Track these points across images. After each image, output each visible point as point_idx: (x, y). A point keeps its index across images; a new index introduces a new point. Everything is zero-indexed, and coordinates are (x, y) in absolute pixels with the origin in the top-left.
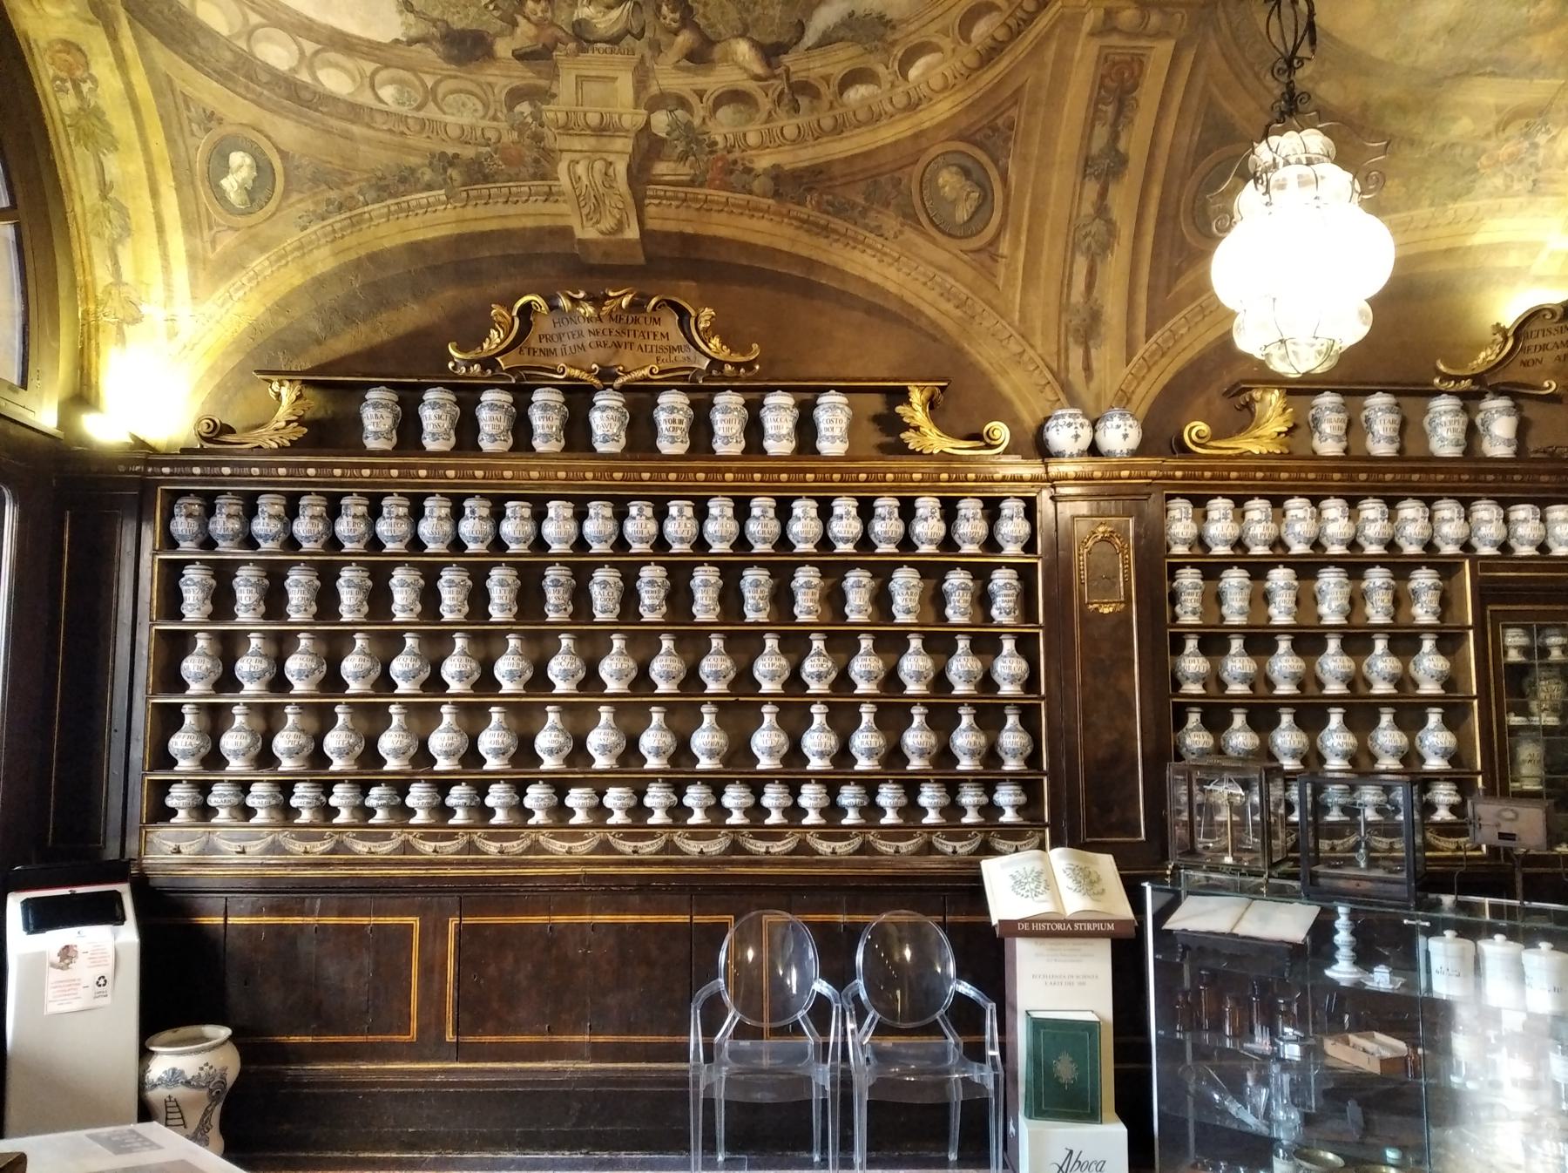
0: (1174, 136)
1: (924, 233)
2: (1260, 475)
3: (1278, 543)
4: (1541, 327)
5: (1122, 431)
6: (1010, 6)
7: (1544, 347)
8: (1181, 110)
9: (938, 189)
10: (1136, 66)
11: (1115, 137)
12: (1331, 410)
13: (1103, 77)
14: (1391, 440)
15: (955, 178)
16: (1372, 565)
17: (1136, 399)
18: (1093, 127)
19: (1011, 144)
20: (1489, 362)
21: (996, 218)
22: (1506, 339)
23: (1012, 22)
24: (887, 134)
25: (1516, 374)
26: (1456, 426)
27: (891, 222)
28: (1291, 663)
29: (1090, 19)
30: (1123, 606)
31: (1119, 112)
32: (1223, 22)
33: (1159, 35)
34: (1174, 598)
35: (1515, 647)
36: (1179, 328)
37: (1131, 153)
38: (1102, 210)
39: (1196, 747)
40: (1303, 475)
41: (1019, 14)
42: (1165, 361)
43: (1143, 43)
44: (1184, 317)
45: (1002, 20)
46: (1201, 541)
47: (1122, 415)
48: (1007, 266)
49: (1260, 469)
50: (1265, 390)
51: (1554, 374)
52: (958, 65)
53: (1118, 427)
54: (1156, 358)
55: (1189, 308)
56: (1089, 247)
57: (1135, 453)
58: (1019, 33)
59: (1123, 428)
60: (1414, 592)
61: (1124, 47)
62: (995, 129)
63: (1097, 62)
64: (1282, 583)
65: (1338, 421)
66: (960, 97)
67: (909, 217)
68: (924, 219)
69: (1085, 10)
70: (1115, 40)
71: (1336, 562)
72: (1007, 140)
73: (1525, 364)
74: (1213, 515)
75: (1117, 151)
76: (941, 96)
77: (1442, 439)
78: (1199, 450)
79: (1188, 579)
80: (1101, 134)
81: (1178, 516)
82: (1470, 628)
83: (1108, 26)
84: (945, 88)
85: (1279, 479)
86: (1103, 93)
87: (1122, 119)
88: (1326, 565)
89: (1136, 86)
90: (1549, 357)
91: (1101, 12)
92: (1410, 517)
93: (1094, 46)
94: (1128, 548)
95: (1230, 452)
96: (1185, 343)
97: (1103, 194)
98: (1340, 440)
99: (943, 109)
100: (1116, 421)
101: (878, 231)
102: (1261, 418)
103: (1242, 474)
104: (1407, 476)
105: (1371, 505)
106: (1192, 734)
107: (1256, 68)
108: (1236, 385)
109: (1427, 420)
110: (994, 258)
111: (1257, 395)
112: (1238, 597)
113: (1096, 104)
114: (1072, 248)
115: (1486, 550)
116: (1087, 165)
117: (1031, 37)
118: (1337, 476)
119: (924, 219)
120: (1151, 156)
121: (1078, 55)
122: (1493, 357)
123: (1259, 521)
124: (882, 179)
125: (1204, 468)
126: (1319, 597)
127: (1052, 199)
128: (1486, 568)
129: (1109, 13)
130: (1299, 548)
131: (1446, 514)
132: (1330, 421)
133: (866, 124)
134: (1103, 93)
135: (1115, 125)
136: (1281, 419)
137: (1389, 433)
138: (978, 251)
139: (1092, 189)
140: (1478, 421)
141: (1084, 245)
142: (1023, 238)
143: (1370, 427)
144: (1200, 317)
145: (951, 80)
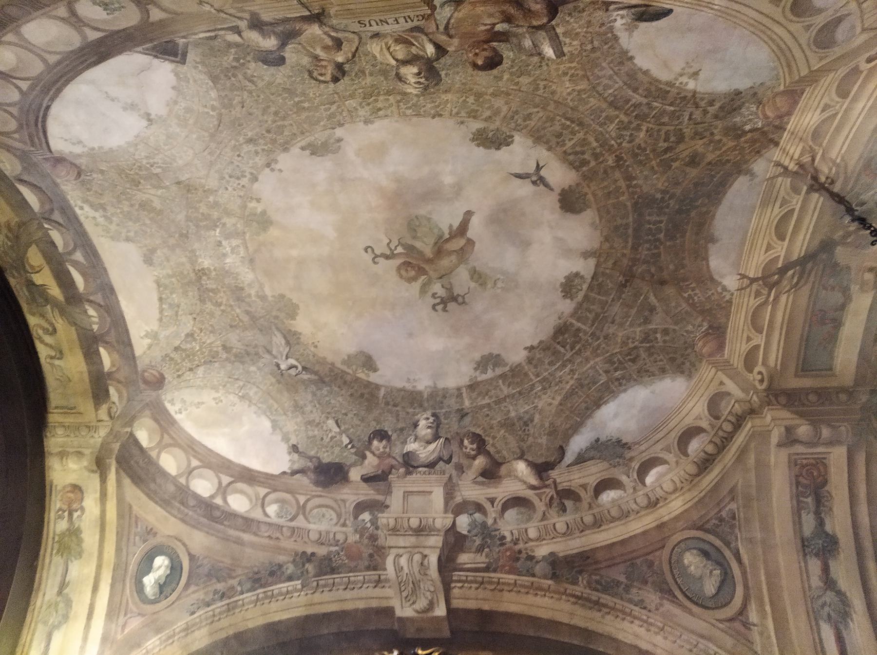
1: (680, 605)
9: (685, 568)
11: (821, 523)
15: (698, 559)
19: (737, 531)
21: (740, 591)
24: (636, 526)
27: (652, 597)
29: (776, 436)
31: (819, 501)
33: (831, 443)
38: (829, 583)
43: (820, 449)
48: (761, 634)
52: (682, 473)
62: (721, 520)
66: (688, 496)
67: (666, 592)
68: (678, 593)
70: (800, 449)
72: (732, 527)
76: (673, 496)
83: (790, 439)
84: (675, 490)
89: (825, 482)
99: (676, 506)
101: (641, 604)
110: (747, 625)
114: (814, 617)
116: (804, 545)
119: (678, 593)
124: (638, 561)
127: (783, 571)
129: (789, 430)
133: (619, 519)
135: (817, 513)
138: (731, 620)
139: (815, 565)
142: (768, 608)
145: (679, 485)
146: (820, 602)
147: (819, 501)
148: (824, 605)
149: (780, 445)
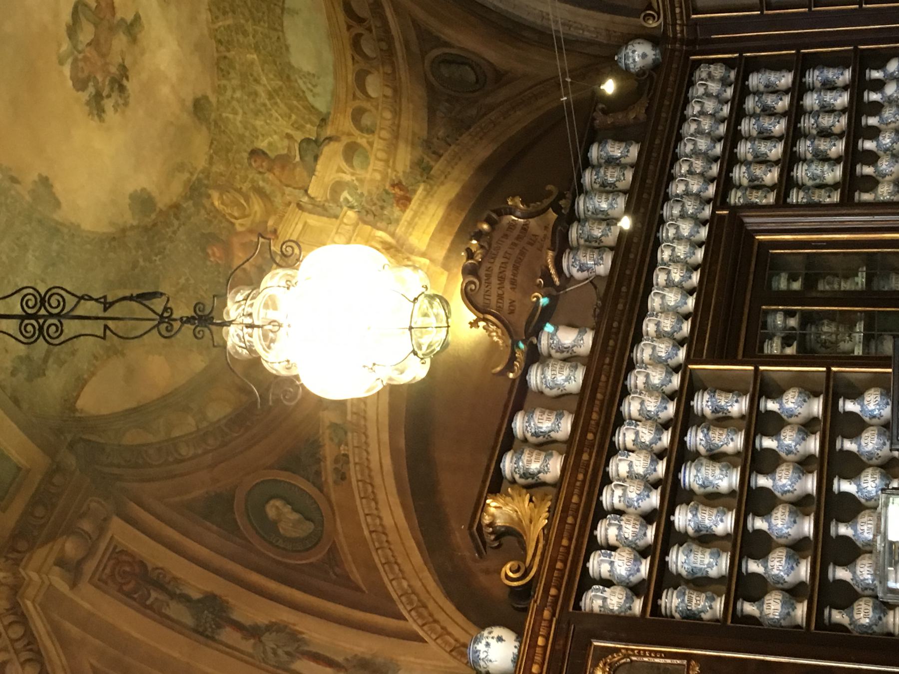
0: (206, 547)
2: (570, 520)
3: (648, 517)
4: (482, 297)
5: (493, 642)
6: (9, 652)
7: (500, 297)
8: (186, 533)
10: (125, 558)
11: (185, 599)
12: (519, 459)
13: (120, 590)
14: (560, 416)
16: (683, 443)
17: (463, 637)
18: (168, 618)
20: (503, 334)
22: (484, 320)
23: (25, 655)
25: (520, 321)
26: (558, 367)
28: (779, 515)
30: (693, 663)
31: (159, 586)
32: (116, 471)
33: (102, 529)
34: (691, 617)
35: (783, 348)
36: (402, 588)
37: (209, 589)
38: (253, 632)
39: (871, 614)
40: (578, 484)
41: (19, 645)
42: (431, 605)
43: (103, 546)
44: (391, 581)
45: (17, 665)
46: (635, 589)
47: (477, 640)
49: (563, 521)
50: (487, 512)
51: (527, 293)
53: (488, 645)
54: (426, 613)
55: (383, 574)
56: (288, 653)
57: (519, 636)
58: (39, 652)
59: (490, 640)
60: (715, 411)
61: (100, 561)
63: (105, 592)
64: (690, 516)
65: (531, 454)
69: (47, 583)
70: (90, 567)
71: (674, 470)
73: (512, 312)
74: (605, 570)
75: (199, 601)
77: (568, 379)
78: (532, 574)
79: (672, 601)
80: (175, 610)
81: (600, 602)
82: (756, 369)
85: (578, 505)
86: (136, 596)
87: (170, 587)
88: (676, 481)
89: (142, 564)
90: (509, 294)
91: (57, 569)
92: (639, 407)
93: (86, 587)
94: (627, 649)
95: (541, 546)
96: (418, 585)
97: (238, 626)
98: (551, 455)
100: (481, 647)
102: (512, 519)
103: (566, 534)
104: (597, 402)
105: (621, 438)
106: (856, 617)
107: (171, 459)
108: (472, 535)
109: (547, 391)
111: (487, 520)
112: (700, 556)
113: (147, 607)
115: (682, 354)
117: (48, 643)
118: (585, 457)
120: (218, 572)
121: (87, 605)
122: (499, 331)
123: (620, 528)
125: (552, 568)
126: (710, 489)
128: (699, 352)
129: (61, 563)
130: (654, 500)
131: (641, 380)
132: (529, 462)
134: (136, 596)
135: (172, 596)
136: (517, 498)
137: (553, 418)
139: (229, 635)
140: (558, 355)
141: (285, 658)
143: (544, 434)
144: (396, 567)
146: (271, 655)
147: (159, 586)
148: (275, 653)
149: (73, 585)
